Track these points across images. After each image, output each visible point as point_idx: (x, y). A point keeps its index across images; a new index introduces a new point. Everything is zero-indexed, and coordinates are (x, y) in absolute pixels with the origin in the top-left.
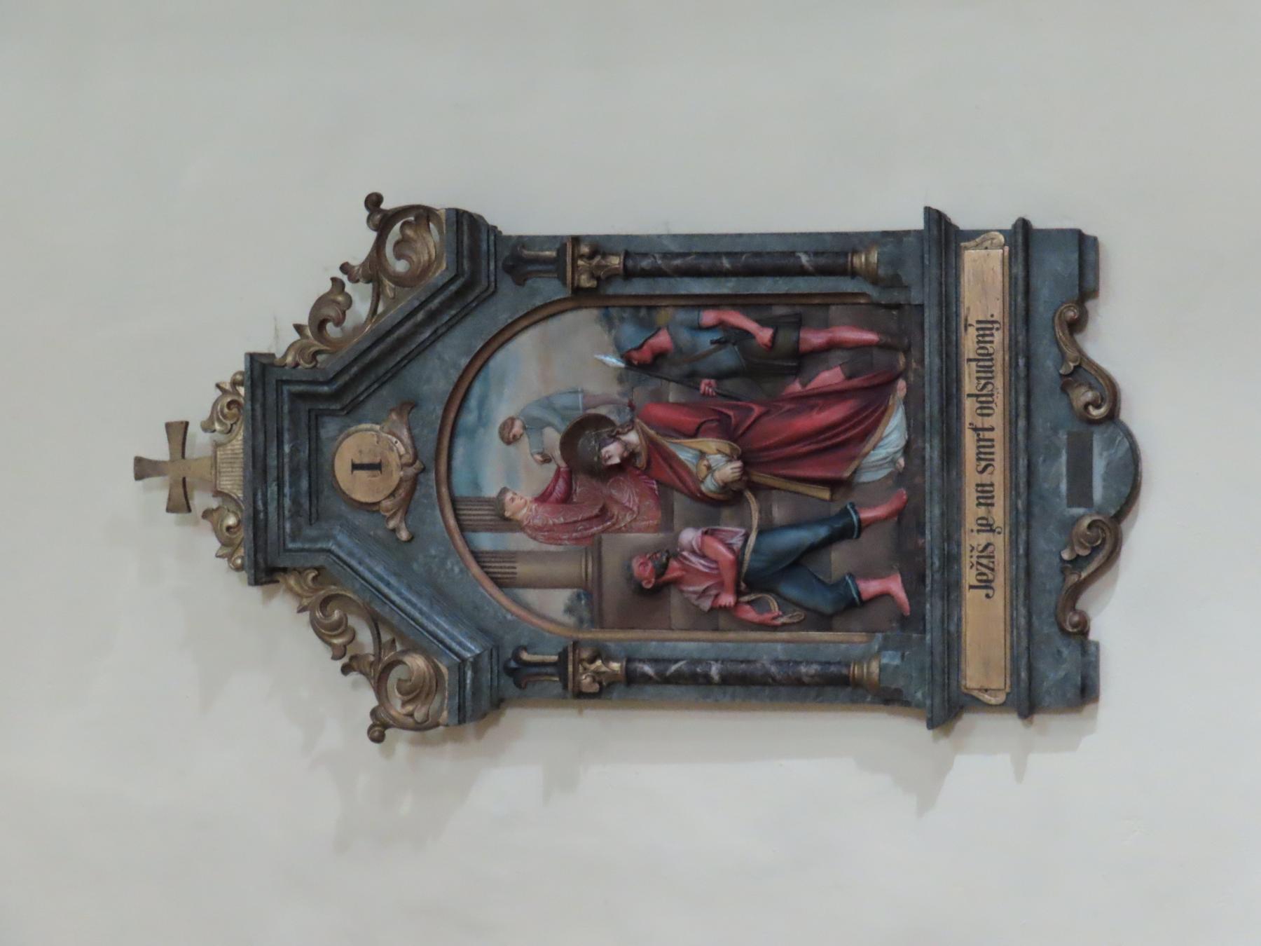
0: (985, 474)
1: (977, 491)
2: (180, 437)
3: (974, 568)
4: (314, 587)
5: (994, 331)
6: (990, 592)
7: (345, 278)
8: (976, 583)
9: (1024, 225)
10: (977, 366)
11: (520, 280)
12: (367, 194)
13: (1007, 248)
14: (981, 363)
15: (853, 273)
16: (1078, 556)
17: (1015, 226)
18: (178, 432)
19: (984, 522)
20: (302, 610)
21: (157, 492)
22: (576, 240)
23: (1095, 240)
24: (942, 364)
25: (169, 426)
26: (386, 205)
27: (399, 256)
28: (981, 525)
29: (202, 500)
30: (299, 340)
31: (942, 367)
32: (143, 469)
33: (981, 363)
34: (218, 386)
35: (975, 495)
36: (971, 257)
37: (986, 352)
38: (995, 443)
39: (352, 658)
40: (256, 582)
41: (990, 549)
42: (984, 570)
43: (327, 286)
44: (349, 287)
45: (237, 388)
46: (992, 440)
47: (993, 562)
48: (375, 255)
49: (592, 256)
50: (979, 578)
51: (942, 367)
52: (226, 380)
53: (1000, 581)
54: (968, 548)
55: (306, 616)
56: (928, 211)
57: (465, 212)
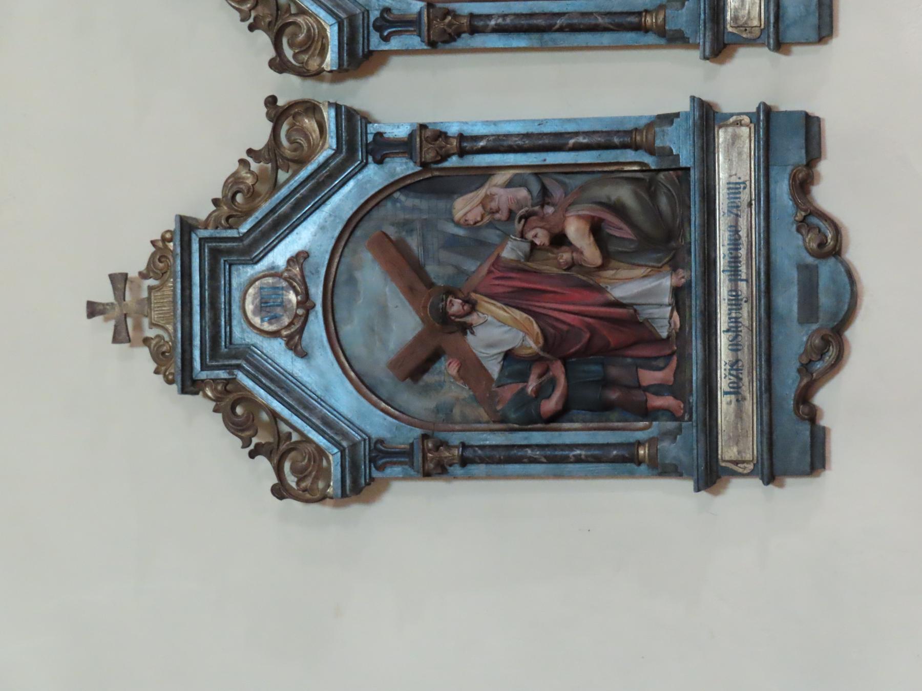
1: (729, 305)
2: (125, 326)
3: (727, 378)
4: (225, 225)
5: (741, 190)
7: (250, 160)
8: (728, 390)
12: (264, 104)
13: (752, 126)
17: (758, 108)
18: (119, 281)
19: (735, 385)
21: (104, 328)
22: (423, 127)
23: (818, 119)
24: (703, 155)
25: (112, 277)
26: (281, 102)
30: (214, 212)
31: (703, 157)
32: (93, 310)
34: (153, 243)
35: (726, 191)
36: (722, 136)
37: (735, 205)
39: (255, 18)
40: (184, 391)
45: (168, 244)
48: (273, 142)
51: (703, 157)
54: (723, 363)
56: (693, 98)
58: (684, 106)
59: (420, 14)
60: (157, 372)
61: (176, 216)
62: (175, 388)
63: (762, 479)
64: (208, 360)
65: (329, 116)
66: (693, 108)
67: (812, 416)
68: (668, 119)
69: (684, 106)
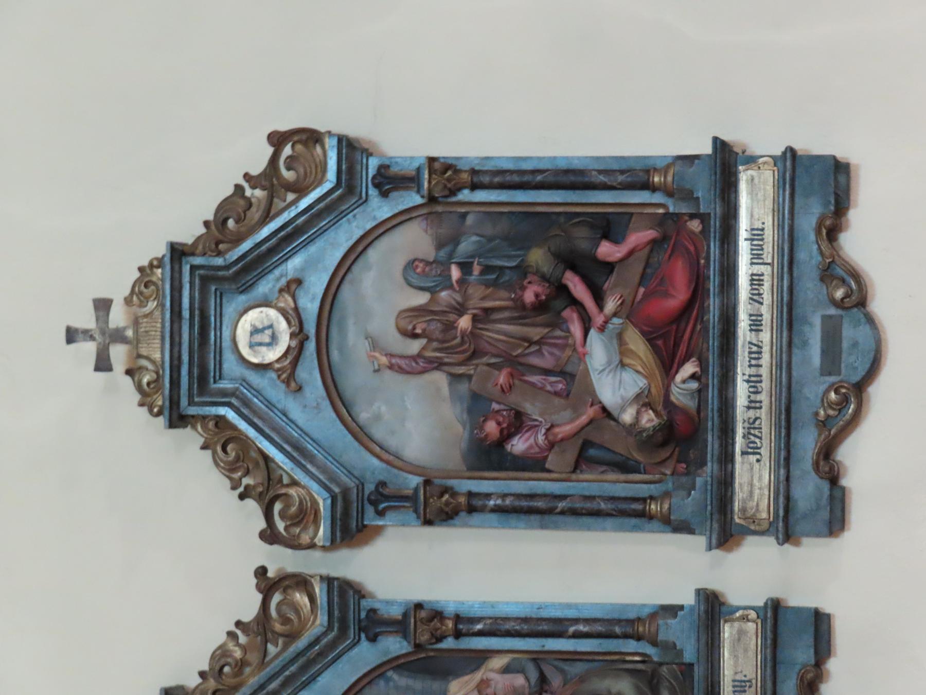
0: (754, 417)
1: (752, 254)
3: (746, 438)
6: (758, 457)
7: (246, 185)
9: (791, 153)
10: (752, 245)
11: (373, 639)
14: (755, 242)
15: (653, 189)
16: (828, 416)
17: (784, 153)
18: (103, 306)
20: (204, 447)
27: (289, 168)
28: (751, 448)
29: (119, 354)
32: (72, 336)
33: (755, 242)
36: (744, 177)
38: (762, 378)
40: (172, 425)
41: (757, 422)
42: (752, 438)
43: (230, 191)
44: (248, 192)
46: (761, 402)
47: (763, 298)
49: (431, 619)
50: (752, 292)
52: (145, 263)
53: (764, 451)
55: (203, 230)
56: (715, 140)
57: (343, 136)
58: (687, 599)
59: (416, 490)
60: (141, 405)
61: (167, 243)
62: (161, 421)
63: (777, 538)
64: (195, 392)
65: (319, 590)
66: (698, 601)
67: (833, 478)
68: (672, 610)
69: (687, 599)
